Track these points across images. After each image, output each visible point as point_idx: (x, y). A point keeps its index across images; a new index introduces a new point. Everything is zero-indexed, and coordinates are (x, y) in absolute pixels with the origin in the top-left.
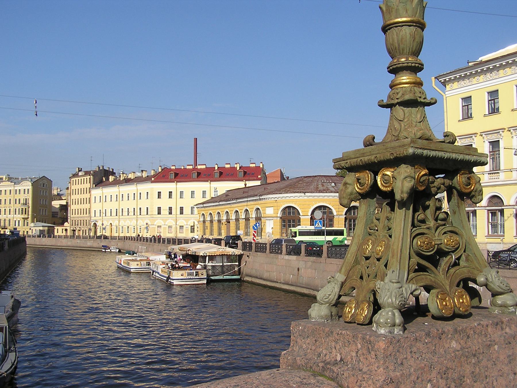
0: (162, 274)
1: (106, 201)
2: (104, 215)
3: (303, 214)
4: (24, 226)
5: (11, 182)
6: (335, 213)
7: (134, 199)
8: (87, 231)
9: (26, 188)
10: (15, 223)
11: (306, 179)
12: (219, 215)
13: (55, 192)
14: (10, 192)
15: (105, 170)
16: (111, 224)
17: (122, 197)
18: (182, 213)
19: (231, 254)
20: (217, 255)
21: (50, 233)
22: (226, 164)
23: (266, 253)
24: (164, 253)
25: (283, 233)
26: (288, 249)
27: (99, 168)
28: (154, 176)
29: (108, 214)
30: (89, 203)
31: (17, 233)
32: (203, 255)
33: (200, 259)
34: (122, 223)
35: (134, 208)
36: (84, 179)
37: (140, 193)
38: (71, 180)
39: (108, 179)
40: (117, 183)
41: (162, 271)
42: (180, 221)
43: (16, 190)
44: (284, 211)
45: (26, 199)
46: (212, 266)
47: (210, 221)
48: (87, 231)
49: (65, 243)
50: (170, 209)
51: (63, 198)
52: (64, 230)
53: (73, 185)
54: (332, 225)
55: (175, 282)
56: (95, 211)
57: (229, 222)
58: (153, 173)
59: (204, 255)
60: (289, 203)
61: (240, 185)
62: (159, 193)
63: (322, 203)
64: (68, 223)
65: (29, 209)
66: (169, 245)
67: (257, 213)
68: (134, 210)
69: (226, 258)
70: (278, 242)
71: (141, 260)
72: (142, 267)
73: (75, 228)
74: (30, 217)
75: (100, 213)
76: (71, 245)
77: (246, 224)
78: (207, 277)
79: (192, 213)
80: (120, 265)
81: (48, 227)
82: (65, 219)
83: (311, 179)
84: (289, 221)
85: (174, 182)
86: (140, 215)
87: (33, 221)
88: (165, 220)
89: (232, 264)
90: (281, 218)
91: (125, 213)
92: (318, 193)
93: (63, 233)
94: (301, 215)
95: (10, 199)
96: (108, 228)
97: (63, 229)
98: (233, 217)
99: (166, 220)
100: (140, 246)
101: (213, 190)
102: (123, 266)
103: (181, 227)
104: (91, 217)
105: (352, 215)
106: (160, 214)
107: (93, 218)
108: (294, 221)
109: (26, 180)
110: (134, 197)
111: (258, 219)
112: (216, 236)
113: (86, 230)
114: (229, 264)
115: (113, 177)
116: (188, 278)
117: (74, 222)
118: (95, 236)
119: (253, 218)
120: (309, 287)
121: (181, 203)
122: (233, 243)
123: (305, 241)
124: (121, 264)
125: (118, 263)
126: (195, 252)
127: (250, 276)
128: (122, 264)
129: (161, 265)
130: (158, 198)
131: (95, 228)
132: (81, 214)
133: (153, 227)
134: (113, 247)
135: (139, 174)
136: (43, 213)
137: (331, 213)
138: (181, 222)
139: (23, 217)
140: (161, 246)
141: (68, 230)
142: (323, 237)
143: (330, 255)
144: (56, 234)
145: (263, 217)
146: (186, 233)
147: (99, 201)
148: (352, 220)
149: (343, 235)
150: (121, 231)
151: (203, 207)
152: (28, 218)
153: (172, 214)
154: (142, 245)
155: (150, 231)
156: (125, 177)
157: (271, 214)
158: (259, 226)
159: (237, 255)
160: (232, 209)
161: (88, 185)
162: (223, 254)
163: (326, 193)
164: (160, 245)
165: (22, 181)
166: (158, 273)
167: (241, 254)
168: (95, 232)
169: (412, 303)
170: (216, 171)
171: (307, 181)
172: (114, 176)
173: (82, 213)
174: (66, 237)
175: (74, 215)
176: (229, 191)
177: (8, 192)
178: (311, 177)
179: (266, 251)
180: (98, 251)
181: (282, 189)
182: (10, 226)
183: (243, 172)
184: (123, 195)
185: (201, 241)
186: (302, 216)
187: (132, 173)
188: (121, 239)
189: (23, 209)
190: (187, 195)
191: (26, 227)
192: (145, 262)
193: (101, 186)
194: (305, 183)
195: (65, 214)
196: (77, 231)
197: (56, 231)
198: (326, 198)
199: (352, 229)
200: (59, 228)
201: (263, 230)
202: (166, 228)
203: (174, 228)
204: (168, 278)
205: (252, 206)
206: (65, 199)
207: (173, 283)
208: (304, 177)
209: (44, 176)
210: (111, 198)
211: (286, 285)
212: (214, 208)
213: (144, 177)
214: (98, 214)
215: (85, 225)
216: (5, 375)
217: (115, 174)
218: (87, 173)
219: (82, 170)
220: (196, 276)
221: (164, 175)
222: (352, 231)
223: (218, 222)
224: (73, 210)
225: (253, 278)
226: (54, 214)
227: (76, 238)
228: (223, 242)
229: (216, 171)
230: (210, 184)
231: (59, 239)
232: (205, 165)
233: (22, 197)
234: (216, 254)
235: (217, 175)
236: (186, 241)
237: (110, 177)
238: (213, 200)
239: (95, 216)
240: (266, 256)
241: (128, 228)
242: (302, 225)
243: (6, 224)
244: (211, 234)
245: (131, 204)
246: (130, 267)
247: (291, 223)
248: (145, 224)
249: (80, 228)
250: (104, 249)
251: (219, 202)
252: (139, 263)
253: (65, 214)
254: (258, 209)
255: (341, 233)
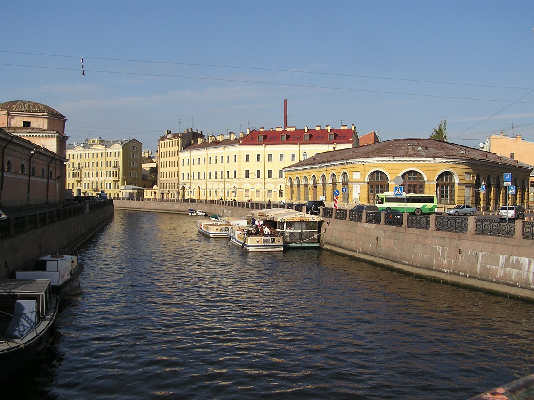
0: (238, 240)
1: (194, 164)
2: (192, 178)
3: (391, 179)
4: (115, 188)
5: (103, 145)
6: (426, 179)
7: (222, 162)
8: (176, 194)
9: (117, 151)
10: (107, 185)
11: (396, 142)
12: (306, 179)
13: (146, 155)
14: (102, 154)
15: (194, 133)
16: (199, 187)
17: (210, 160)
18: (270, 176)
19: (310, 220)
20: (295, 221)
21: (140, 196)
22: (317, 126)
23: (345, 220)
24: (246, 218)
25: (371, 199)
26: (368, 217)
27: (188, 130)
28: (242, 139)
29: (196, 177)
30: (177, 166)
31: (104, 196)
32: (281, 221)
33: (278, 225)
34: (210, 186)
35: (222, 172)
36: (172, 141)
37: (228, 156)
38: (159, 143)
39: (196, 142)
40: (205, 145)
41: (239, 237)
42: (268, 185)
43: (107, 153)
44: (372, 176)
45: (117, 162)
46: (290, 233)
47: (297, 185)
48: (176, 194)
49: (153, 206)
50: (259, 172)
51: (154, 161)
52: (153, 193)
53: (162, 148)
54: (422, 192)
55: (251, 249)
56: (183, 174)
57: (316, 187)
58: (241, 135)
59: (282, 222)
60: (377, 168)
61: (329, 148)
62: (247, 156)
63: (412, 168)
64: (157, 186)
65: (120, 172)
66: (252, 209)
67: (344, 177)
68: (222, 174)
69: (305, 225)
70: (360, 208)
71: (221, 225)
72: (222, 232)
73: (164, 191)
74: (120, 179)
75: (188, 176)
76: (159, 208)
77: (333, 189)
78: (284, 244)
79: (281, 177)
80: (200, 230)
81: (138, 189)
82: (155, 182)
83: (402, 142)
84: (377, 187)
85: (262, 145)
86: (228, 178)
87: (123, 184)
88: (252, 184)
89: (311, 231)
90: (368, 183)
91: (213, 176)
92: (408, 157)
93: (152, 196)
94: (389, 180)
95: (102, 162)
96: (196, 191)
97: (152, 192)
98: (320, 181)
99: (254, 184)
100: (225, 210)
101: (302, 153)
102: (203, 231)
103: (270, 191)
104: (179, 180)
105: (445, 181)
106: (248, 178)
107: (181, 181)
108: (382, 187)
109: (117, 143)
110: (222, 160)
111: (345, 184)
112: (303, 200)
113: (174, 193)
114: (308, 231)
115: (202, 140)
116: (264, 245)
117: (162, 185)
118: (163, 199)
119: (339, 183)
120: (387, 258)
121: (270, 166)
122: (315, 209)
123: (392, 208)
124: (201, 229)
125: (199, 227)
126: (273, 218)
127: (330, 244)
128: (203, 229)
129: (238, 230)
130: (246, 161)
131: (184, 191)
132: (169, 177)
133: (241, 191)
134: (199, 211)
135: (227, 137)
136: (133, 176)
137: (422, 178)
138: (269, 186)
139: (114, 180)
140: (245, 210)
141: (157, 193)
142: (404, 204)
143: (410, 225)
144: (145, 197)
145: (350, 182)
146: (274, 197)
147: (187, 164)
148: (444, 187)
149: (434, 203)
150: (208, 195)
151: (290, 171)
152: (119, 181)
153: (271, 178)
154: (227, 209)
155: (238, 195)
156: (213, 140)
157: (358, 179)
158: (345, 191)
159: (316, 221)
160: (319, 173)
161: (176, 148)
162: (302, 220)
163: (417, 157)
164: (244, 209)
165: (113, 143)
166: (235, 239)
167: (321, 221)
168: (184, 195)
169: (495, 280)
170: (306, 134)
171: (397, 144)
172: (203, 139)
173: (171, 176)
174: (155, 200)
175: (162, 178)
176: (317, 154)
177: (100, 155)
178: (401, 140)
179: (346, 218)
180: (185, 214)
181: (370, 153)
182: (101, 188)
183: (334, 135)
184: (210, 158)
185: (283, 206)
186: (390, 181)
187: (220, 136)
188: (208, 203)
189: (114, 171)
190: (276, 158)
191: (117, 189)
192: (225, 227)
193: (189, 149)
194: (394, 146)
195: (153, 177)
196: (165, 194)
197: (145, 194)
198: (416, 162)
199: (444, 196)
200: (148, 191)
201: (350, 195)
202: (254, 192)
203: (262, 192)
204: (244, 244)
205: (339, 171)
206: (156, 162)
207: (248, 249)
208: (394, 140)
209: (134, 139)
210: (199, 161)
211: (365, 255)
212: (301, 171)
213: (232, 139)
214: (186, 177)
215: (173, 188)
216: (23, 347)
217: (204, 137)
218: (175, 136)
219: (171, 132)
220: (272, 243)
221: (253, 138)
222: (444, 198)
223: (305, 186)
224: (161, 173)
225: (332, 246)
226: (144, 177)
227: (164, 201)
228: (304, 208)
229: (306, 134)
230: (300, 147)
231: (147, 202)
232: (295, 127)
233: (113, 160)
234: (294, 221)
235: (307, 138)
236: (269, 205)
237: (199, 140)
238: (301, 163)
239: (183, 179)
240: (346, 223)
241: (216, 191)
242: (390, 191)
243: (98, 186)
244: (299, 199)
245: (219, 168)
246: (209, 232)
247: (379, 188)
248: (232, 187)
249: (168, 191)
250: (190, 212)
251: (306, 166)
252: (218, 228)
253: (153, 177)
254: (345, 173)
255: (431, 200)
